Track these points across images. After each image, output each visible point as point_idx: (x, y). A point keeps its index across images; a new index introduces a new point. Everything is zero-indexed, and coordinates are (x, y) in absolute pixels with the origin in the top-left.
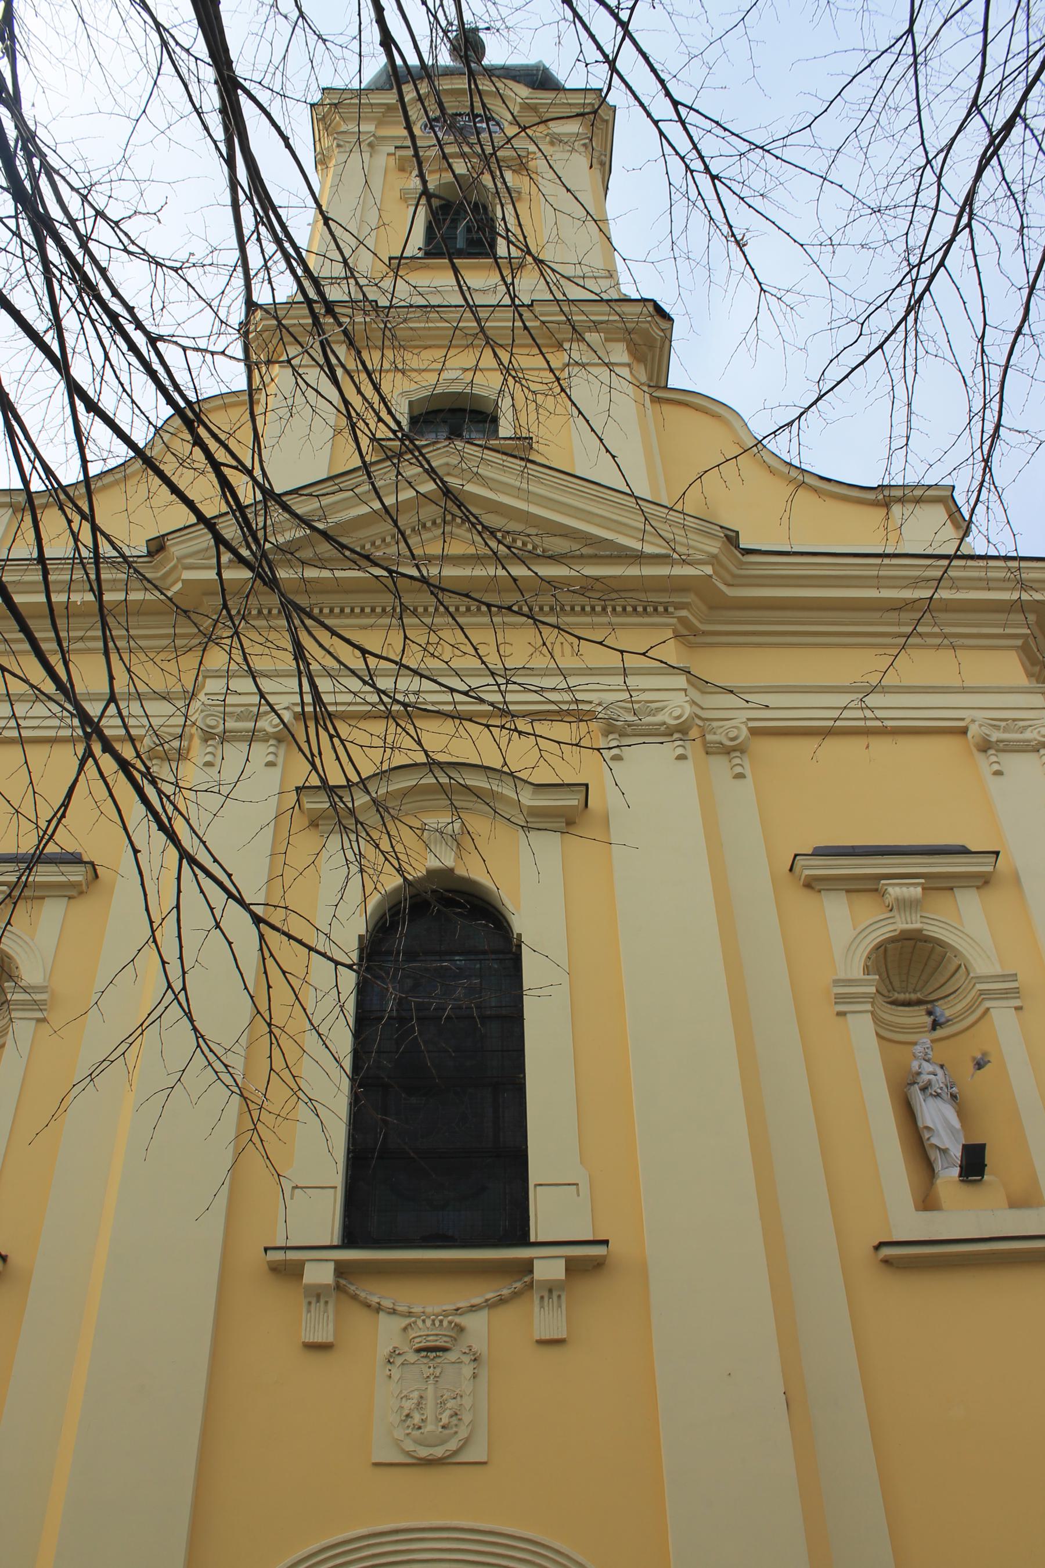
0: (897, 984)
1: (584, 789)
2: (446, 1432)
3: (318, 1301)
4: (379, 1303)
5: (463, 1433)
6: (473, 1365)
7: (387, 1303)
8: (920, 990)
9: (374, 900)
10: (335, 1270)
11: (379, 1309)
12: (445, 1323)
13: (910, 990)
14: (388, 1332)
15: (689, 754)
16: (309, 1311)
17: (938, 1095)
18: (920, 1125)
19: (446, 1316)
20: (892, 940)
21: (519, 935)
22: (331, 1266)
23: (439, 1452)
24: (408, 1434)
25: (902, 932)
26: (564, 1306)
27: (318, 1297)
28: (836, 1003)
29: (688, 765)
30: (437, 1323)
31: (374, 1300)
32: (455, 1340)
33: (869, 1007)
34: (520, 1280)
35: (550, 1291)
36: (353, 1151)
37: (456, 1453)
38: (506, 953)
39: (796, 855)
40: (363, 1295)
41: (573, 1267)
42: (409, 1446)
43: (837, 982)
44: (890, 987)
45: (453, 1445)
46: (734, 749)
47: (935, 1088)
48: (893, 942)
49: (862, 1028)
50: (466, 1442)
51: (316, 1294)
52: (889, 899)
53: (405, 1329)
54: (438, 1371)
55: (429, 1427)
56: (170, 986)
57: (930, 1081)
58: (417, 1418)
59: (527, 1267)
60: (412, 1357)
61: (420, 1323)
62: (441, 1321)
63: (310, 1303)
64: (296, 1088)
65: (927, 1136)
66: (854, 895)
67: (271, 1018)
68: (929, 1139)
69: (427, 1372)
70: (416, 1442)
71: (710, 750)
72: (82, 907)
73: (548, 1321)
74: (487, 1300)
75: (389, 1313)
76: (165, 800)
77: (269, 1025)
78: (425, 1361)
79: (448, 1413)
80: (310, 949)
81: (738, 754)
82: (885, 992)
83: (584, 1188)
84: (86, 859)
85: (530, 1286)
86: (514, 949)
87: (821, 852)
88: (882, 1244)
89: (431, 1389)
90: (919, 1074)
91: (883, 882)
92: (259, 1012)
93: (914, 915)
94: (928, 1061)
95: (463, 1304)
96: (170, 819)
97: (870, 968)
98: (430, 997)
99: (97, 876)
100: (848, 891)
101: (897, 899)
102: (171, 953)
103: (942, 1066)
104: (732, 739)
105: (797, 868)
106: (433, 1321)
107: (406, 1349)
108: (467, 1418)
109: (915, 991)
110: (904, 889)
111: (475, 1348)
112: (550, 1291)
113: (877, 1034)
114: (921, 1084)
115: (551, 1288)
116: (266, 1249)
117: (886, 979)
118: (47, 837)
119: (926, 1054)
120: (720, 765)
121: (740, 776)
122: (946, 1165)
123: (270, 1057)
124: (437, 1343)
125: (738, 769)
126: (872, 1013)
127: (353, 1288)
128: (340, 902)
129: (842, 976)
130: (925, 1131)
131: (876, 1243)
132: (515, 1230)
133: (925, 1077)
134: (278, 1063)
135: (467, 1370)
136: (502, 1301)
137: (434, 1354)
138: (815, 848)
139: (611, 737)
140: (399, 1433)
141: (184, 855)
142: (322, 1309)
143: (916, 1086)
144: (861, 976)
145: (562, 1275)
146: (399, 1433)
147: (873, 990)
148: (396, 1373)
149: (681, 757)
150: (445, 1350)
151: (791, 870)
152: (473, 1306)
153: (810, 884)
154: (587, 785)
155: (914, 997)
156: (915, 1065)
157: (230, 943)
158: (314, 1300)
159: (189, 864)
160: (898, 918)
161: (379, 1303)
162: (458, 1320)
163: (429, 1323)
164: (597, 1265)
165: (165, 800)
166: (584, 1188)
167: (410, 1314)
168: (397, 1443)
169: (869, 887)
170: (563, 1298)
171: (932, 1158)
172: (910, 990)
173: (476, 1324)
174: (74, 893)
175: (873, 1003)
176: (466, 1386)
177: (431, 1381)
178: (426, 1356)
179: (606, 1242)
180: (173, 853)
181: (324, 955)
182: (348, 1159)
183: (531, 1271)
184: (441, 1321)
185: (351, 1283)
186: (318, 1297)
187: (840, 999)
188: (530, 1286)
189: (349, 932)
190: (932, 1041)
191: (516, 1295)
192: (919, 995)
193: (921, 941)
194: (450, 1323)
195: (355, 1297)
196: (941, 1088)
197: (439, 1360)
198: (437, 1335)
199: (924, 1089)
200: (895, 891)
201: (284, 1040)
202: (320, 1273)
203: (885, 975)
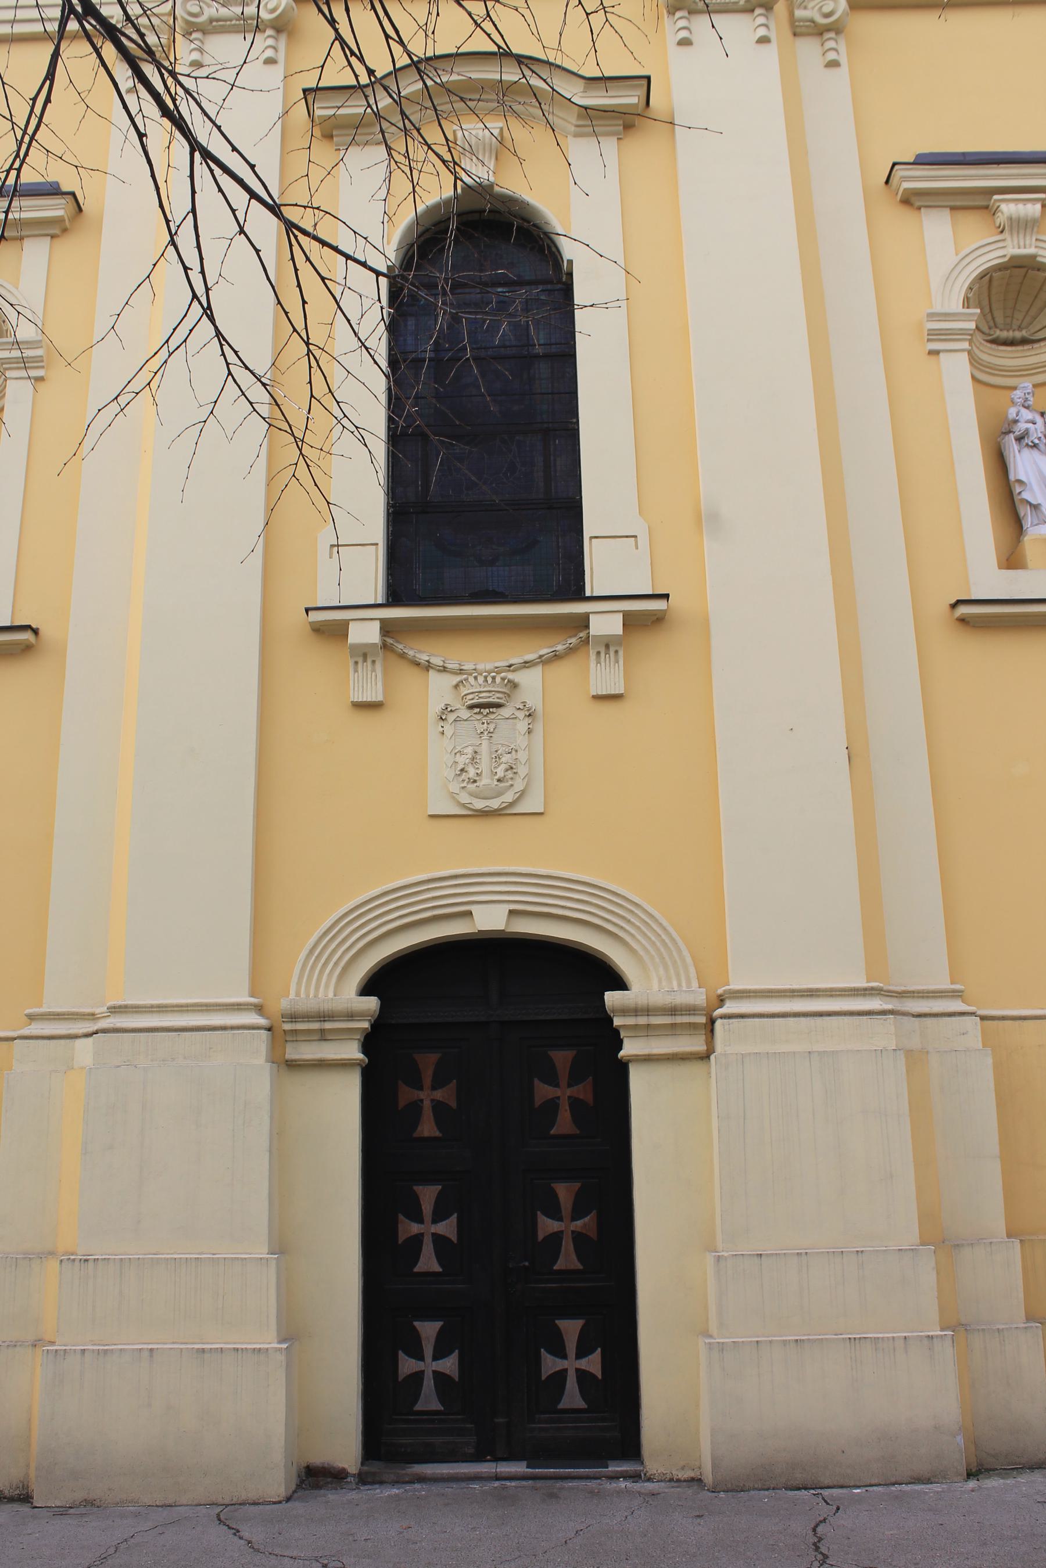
0: (1000, 320)
1: (645, 82)
2: (502, 785)
3: (365, 660)
4: (428, 661)
5: (519, 786)
6: (528, 720)
7: (437, 661)
8: (1027, 327)
9: (406, 217)
10: (381, 628)
11: (428, 667)
12: (498, 680)
13: (1015, 327)
14: (439, 689)
15: (773, 36)
16: (356, 671)
17: (1035, 446)
18: (1012, 478)
19: (498, 673)
20: (1000, 268)
21: (570, 262)
22: (377, 625)
23: (495, 804)
24: (463, 788)
25: (1013, 258)
26: (621, 662)
27: (365, 656)
28: (928, 340)
29: (771, 52)
30: (490, 680)
31: (423, 657)
32: (509, 696)
33: (966, 345)
34: (575, 636)
35: (607, 646)
36: (393, 506)
37: (511, 805)
38: (558, 287)
39: (894, 164)
40: (411, 653)
41: (631, 621)
42: (464, 798)
43: (932, 316)
44: (992, 324)
45: (509, 797)
46: (828, 29)
47: (1033, 438)
48: (1000, 270)
49: (956, 368)
50: (522, 794)
51: (363, 653)
52: (1001, 219)
53: (456, 686)
54: (491, 727)
55: (485, 781)
56: (195, 296)
57: (1027, 430)
58: (472, 772)
59: (583, 622)
60: (465, 714)
61: (471, 679)
62: (494, 678)
63: (356, 663)
64: (340, 415)
65: (1018, 491)
66: (960, 215)
67: (308, 338)
68: (1020, 493)
69: (481, 728)
70: (471, 794)
71: (798, 30)
72: (69, 248)
73: (605, 676)
74: (541, 657)
75: (439, 671)
76: (166, 75)
77: (307, 344)
78: (478, 717)
79: (503, 767)
80: (348, 257)
81: (832, 35)
82: (985, 329)
83: (643, 540)
84: (65, 188)
85: (586, 641)
86: (564, 279)
87: (924, 160)
88: (959, 602)
89: (485, 743)
90: (1016, 421)
91: (996, 197)
92: (295, 330)
93: (1028, 238)
94: (1027, 408)
95: (516, 660)
96: (174, 100)
97: (971, 301)
98: (483, 313)
99: (80, 210)
100: (953, 208)
101: (1010, 219)
102: (191, 259)
103: (1042, 414)
104: (827, 15)
105: (895, 180)
106: (486, 677)
107: (459, 706)
108: (522, 771)
109: (1020, 328)
110: (1021, 206)
111: (529, 704)
112: (607, 646)
113: (973, 377)
114: (1017, 433)
115: (608, 644)
116: (307, 610)
117: (988, 315)
118: (27, 139)
119: (1026, 400)
120: (809, 50)
121: (834, 64)
122: (1036, 522)
123: (310, 382)
124: (491, 700)
125: (832, 56)
126: (969, 352)
127: (400, 646)
128: (373, 205)
129: (938, 308)
130: (1017, 485)
131: (953, 601)
132: (571, 585)
133: (1022, 426)
134: (320, 389)
135: (522, 726)
136: (556, 657)
137: (487, 710)
138: (918, 156)
139: (678, 14)
140: (454, 787)
141: (195, 146)
142: (369, 668)
143: (1012, 436)
144: (960, 309)
145: (619, 630)
146: (454, 787)
147: (972, 325)
148: (449, 730)
149: (764, 40)
150: (498, 706)
151: (887, 182)
152: (526, 662)
153: (910, 200)
154: (649, 78)
155: (1018, 335)
156: (1012, 412)
157: (257, 251)
158: (360, 660)
159: (202, 156)
160: (1009, 242)
161: (428, 661)
162: (511, 676)
163: (481, 679)
164: (657, 619)
165: (166, 75)
166: (643, 540)
167: (461, 671)
168: (453, 796)
169: (978, 203)
170: (621, 653)
171: (1022, 514)
172: (1015, 327)
173: (530, 681)
174: (57, 231)
175: (971, 341)
176: (522, 741)
177: (485, 736)
178: (480, 713)
179: (666, 596)
180: (181, 147)
181: (364, 264)
182: (388, 514)
183: (587, 627)
184: (494, 678)
185: (398, 642)
186: (365, 656)
187: (934, 335)
188: (586, 641)
189: (386, 249)
190: (1034, 386)
191: (571, 651)
192: (1024, 333)
193: (1033, 269)
194: (503, 679)
195: (403, 656)
196: (1039, 439)
197: (492, 716)
198: (489, 691)
199: (1019, 439)
200: (1009, 208)
201: (324, 360)
202: (365, 632)
203: (987, 310)
